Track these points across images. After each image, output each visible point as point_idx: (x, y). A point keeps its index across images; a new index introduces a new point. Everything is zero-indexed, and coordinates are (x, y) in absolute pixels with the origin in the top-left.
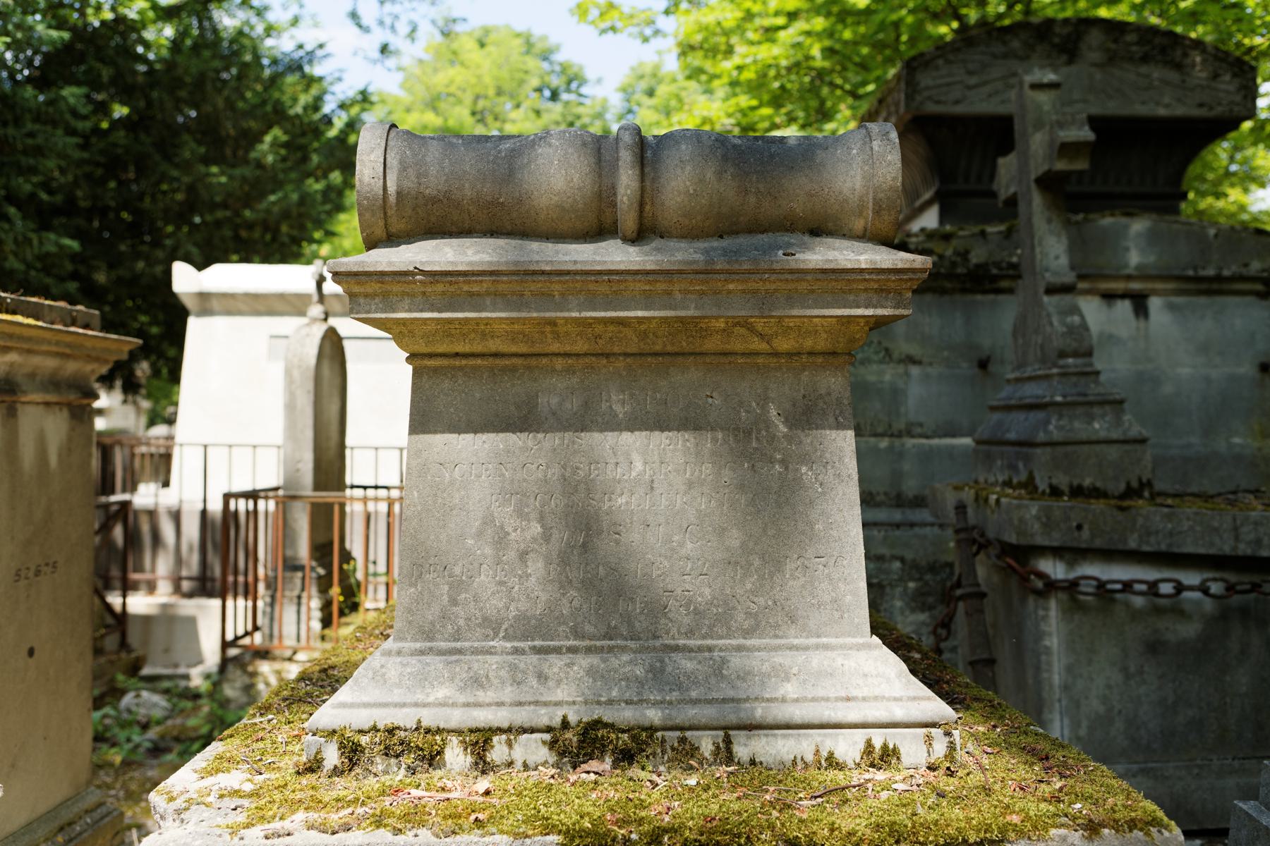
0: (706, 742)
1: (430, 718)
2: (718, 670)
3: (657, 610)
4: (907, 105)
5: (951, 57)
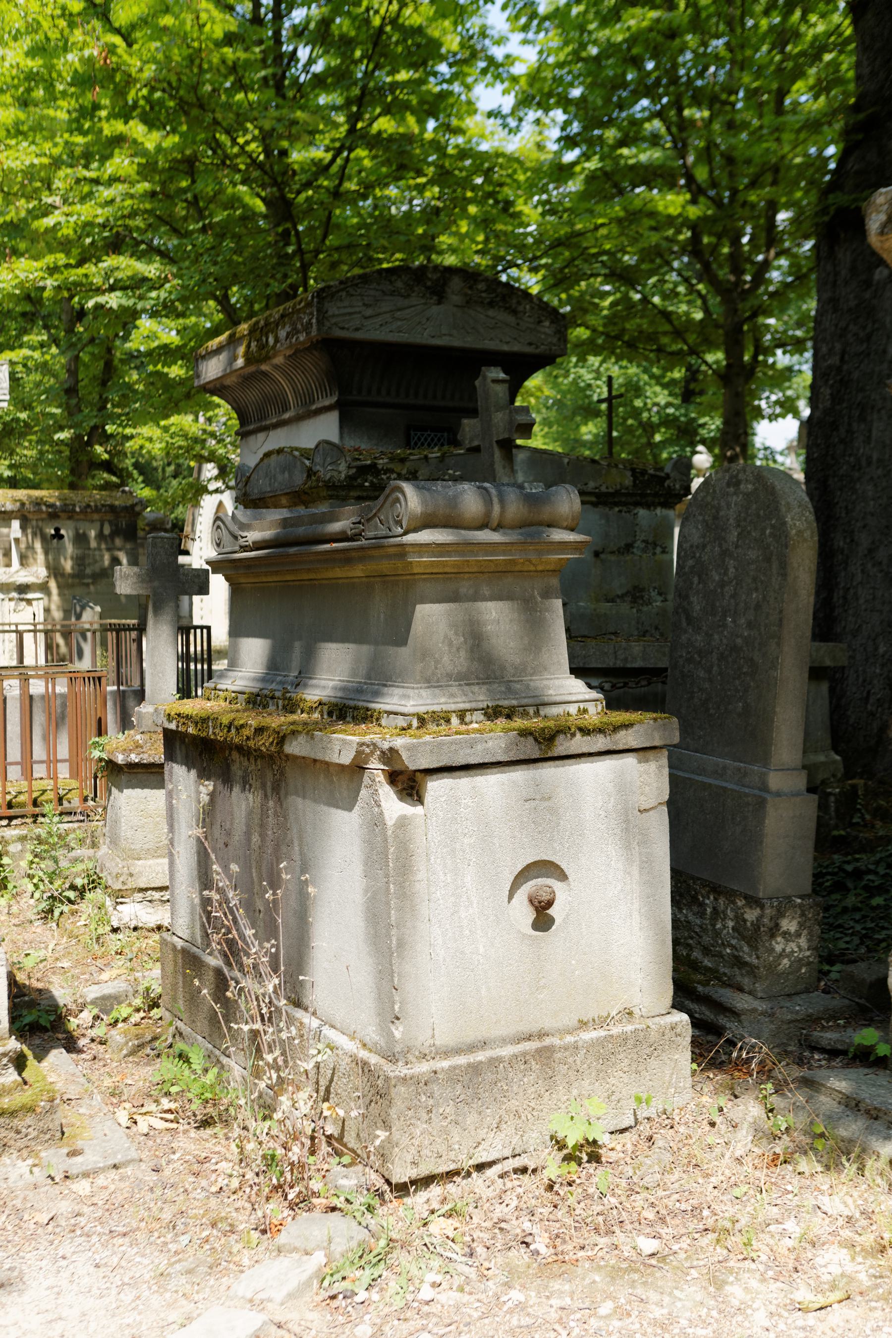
0: (531, 710)
1: (445, 708)
2: (528, 686)
3: (503, 668)
4: (319, 330)
5: (352, 291)
